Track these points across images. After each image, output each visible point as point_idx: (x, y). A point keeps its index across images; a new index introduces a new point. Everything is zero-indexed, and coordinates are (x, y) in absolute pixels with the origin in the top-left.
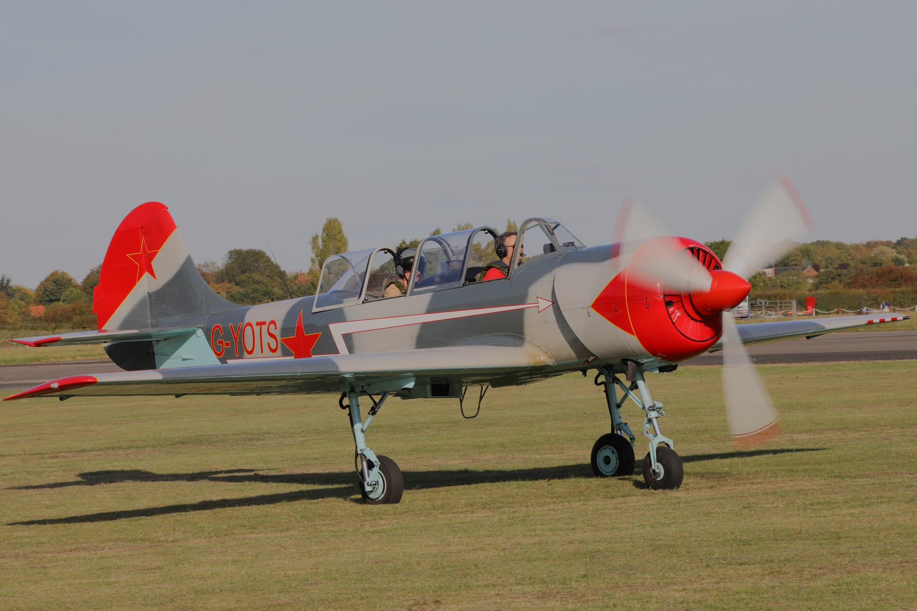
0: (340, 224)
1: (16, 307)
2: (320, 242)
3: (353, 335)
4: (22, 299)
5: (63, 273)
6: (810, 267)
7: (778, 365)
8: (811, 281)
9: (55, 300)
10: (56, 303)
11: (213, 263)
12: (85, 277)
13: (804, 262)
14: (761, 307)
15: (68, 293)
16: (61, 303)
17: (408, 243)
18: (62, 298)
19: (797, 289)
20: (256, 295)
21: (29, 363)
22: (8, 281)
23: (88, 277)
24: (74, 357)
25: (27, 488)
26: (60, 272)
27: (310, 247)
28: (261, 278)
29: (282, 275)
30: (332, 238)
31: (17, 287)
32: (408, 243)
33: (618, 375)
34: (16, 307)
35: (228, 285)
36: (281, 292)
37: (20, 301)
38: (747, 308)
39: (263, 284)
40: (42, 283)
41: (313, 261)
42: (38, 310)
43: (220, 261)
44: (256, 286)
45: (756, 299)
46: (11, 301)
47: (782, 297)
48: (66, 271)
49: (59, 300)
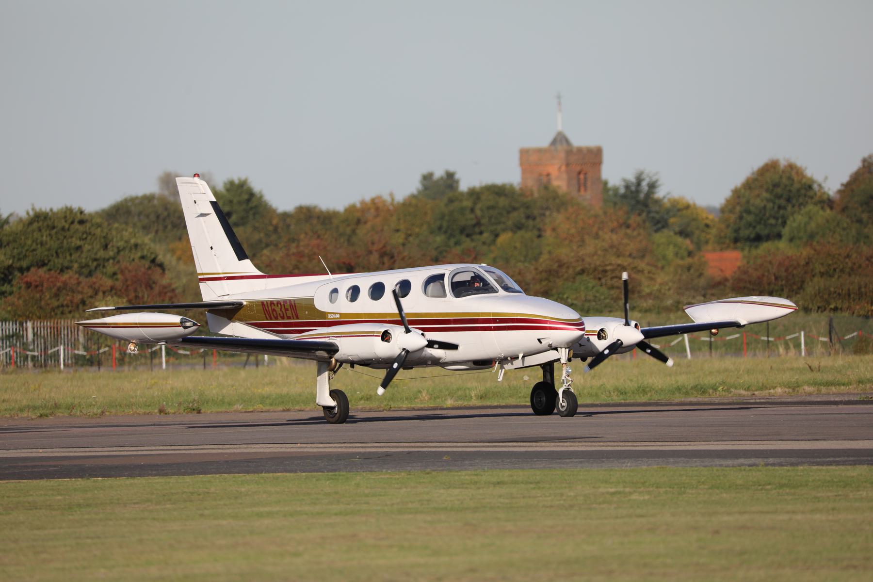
3: (333, 388)
4: (683, 233)
5: (791, 166)
9: (768, 238)
10: (765, 246)
12: (845, 179)
16: (782, 244)
21: (678, 398)
22: (652, 186)
24: (795, 387)
25: (154, 425)
26: (783, 163)
33: (332, 403)
37: (679, 240)
40: (736, 193)
42: (729, 261)
48: (799, 163)
49: (779, 236)
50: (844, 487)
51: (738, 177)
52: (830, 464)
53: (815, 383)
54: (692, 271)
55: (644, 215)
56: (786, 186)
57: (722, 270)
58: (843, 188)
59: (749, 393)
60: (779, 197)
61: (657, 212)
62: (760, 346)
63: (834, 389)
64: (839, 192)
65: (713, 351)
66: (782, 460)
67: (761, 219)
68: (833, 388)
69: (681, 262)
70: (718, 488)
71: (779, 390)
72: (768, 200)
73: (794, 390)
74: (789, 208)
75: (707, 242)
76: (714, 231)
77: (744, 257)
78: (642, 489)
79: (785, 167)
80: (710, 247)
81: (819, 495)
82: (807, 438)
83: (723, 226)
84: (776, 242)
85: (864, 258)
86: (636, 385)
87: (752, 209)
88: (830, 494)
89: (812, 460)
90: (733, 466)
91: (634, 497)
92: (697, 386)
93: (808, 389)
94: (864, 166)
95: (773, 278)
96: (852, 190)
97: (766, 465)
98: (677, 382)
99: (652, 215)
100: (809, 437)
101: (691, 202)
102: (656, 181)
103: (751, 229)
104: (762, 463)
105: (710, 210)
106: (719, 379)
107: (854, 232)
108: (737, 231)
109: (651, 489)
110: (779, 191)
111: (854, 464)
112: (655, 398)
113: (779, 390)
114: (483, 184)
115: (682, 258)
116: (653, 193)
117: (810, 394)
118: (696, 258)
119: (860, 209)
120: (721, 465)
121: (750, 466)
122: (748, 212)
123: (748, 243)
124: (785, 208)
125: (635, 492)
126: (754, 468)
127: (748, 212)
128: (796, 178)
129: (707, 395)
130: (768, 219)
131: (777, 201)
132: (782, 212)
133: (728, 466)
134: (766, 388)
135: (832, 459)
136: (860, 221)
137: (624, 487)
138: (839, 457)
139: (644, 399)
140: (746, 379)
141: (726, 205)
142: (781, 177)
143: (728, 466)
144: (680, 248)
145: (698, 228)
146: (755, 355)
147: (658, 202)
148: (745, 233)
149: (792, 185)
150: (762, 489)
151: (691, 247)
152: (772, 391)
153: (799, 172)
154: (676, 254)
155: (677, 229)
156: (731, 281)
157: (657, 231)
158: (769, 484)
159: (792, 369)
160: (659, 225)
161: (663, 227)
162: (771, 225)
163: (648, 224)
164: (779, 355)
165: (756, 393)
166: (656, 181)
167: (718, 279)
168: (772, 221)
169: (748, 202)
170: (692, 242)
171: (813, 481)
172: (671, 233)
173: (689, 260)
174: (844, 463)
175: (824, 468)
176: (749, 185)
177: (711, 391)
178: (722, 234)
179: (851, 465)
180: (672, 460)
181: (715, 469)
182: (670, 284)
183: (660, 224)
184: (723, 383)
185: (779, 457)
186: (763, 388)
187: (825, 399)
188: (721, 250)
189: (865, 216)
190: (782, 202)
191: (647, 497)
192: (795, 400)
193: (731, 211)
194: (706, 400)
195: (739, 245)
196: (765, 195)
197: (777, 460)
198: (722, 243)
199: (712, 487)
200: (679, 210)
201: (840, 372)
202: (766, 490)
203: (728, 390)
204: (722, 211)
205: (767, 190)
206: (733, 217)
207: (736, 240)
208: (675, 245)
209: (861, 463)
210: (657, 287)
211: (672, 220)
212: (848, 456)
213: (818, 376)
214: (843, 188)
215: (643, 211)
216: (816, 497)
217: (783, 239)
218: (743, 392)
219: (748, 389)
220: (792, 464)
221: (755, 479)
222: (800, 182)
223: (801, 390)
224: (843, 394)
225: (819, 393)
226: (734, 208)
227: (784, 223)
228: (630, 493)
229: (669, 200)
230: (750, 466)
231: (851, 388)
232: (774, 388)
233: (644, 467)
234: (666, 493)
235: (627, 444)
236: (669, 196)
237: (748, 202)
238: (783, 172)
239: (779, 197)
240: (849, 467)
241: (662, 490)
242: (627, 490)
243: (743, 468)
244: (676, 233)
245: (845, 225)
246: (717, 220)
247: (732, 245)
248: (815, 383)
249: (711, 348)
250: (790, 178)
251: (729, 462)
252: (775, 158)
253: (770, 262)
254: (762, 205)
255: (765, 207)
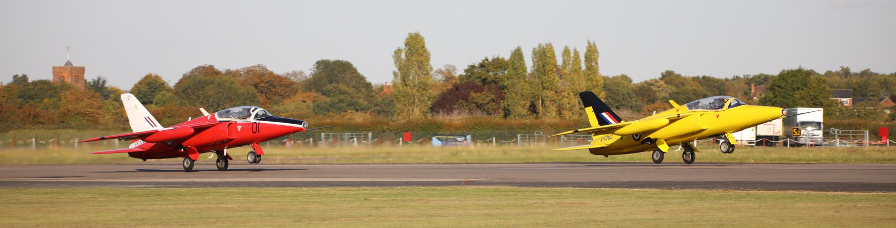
0: (422, 39)
1: (110, 107)
2: (403, 56)
5: (157, 76)
6: (887, 98)
7: (840, 193)
8: (888, 112)
11: (301, 73)
13: (882, 93)
14: (834, 135)
15: (160, 96)
17: (490, 60)
18: (154, 101)
19: (874, 119)
20: (341, 105)
22: (104, 82)
23: (181, 81)
27: (392, 61)
28: (347, 89)
29: (368, 86)
30: (415, 51)
31: (112, 88)
32: (490, 60)
34: (110, 107)
35: (315, 94)
36: (366, 102)
38: (821, 136)
39: (349, 94)
40: (136, 85)
41: (395, 74)
43: (307, 69)
44: (342, 97)
45: (829, 127)
46: (106, 102)
47: (857, 127)
49: (152, 102)
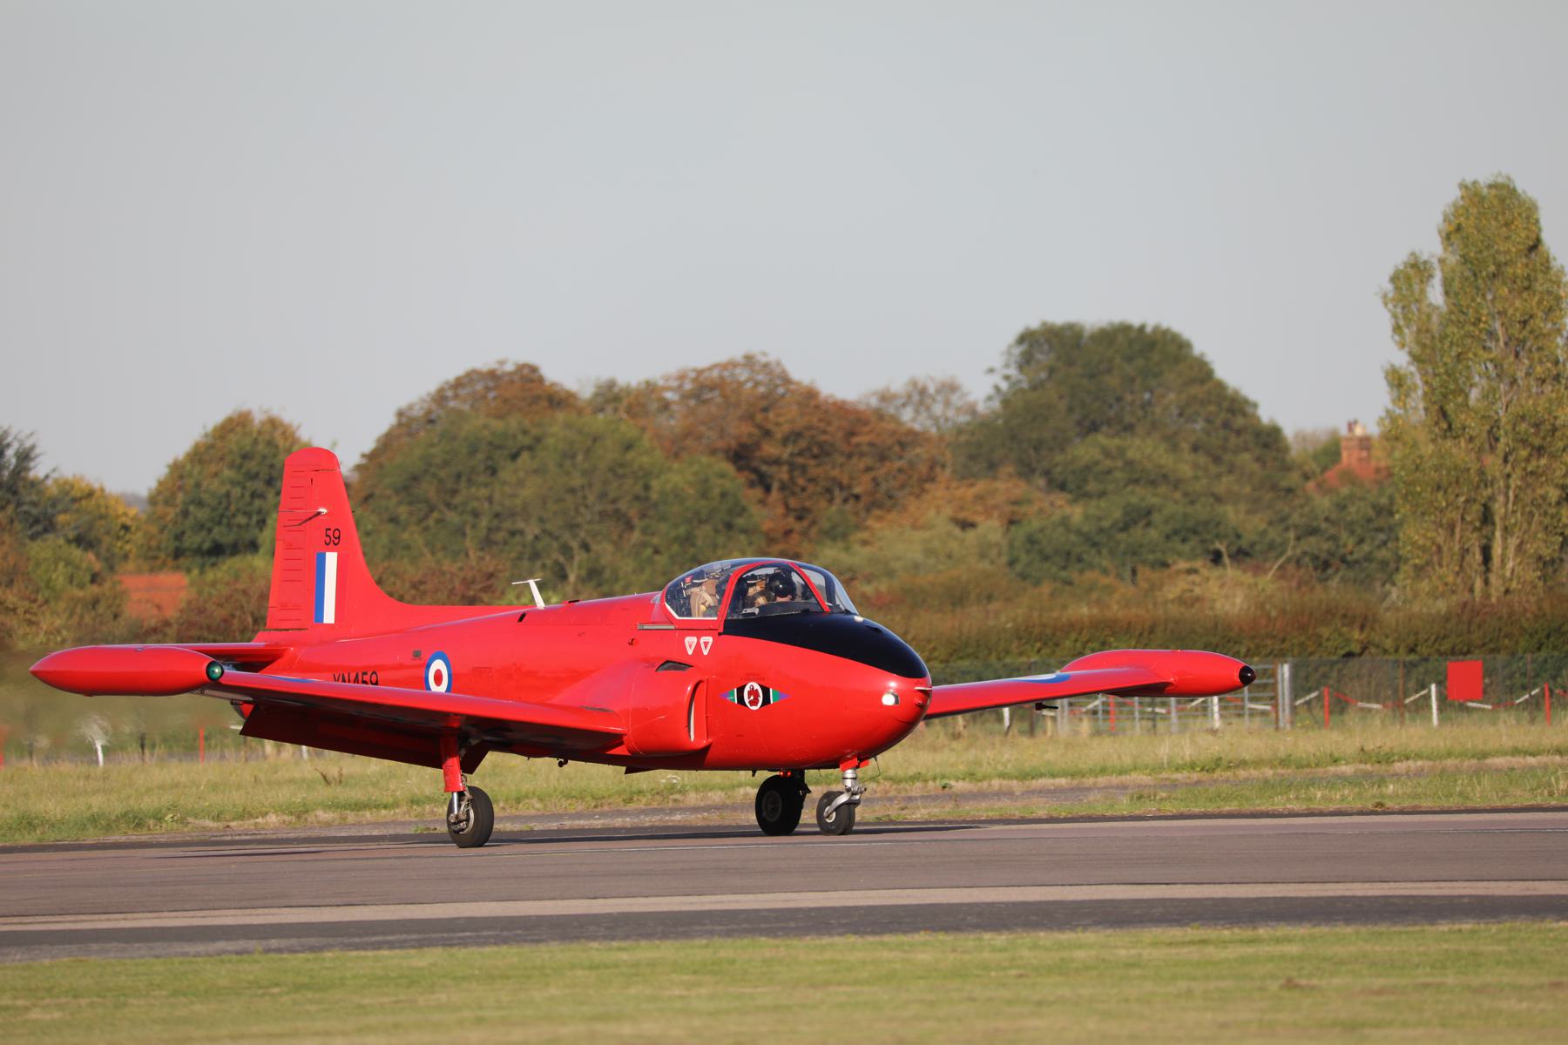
4: (83, 541)
9: (235, 549)
10: (229, 565)
12: (369, 446)
24: (301, 812)
26: (258, 417)
37: (76, 553)
40: (177, 470)
49: (253, 546)
50: (409, 986)
51: (180, 442)
52: (378, 946)
53: (335, 806)
54: (101, 609)
55: (10, 509)
56: (264, 457)
57: (159, 607)
58: (364, 461)
59: (221, 825)
60: (254, 477)
61: (34, 504)
62: (228, 741)
63: (368, 815)
64: (358, 468)
65: (147, 751)
66: (293, 941)
67: (222, 516)
68: (368, 814)
69: (80, 594)
70: (185, 995)
71: (273, 819)
72: (233, 483)
73: (299, 817)
74: (271, 495)
75: (126, 557)
76: (138, 537)
77: (192, 584)
78: (47, 1001)
79: (263, 423)
80: (130, 565)
81: (366, 1001)
82: (333, 901)
83: (154, 529)
84: (249, 557)
85: (407, 585)
86: (15, 815)
87: (205, 497)
88: (385, 1000)
89: (346, 940)
90: (209, 955)
91: (35, 1014)
92: (126, 814)
93: (323, 815)
94: (400, 425)
95: (250, 620)
96: (381, 466)
97: (267, 951)
98: (90, 807)
99: (25, 508)
100: (339, 901)
101: (96, 486)
102: (33, 448)
103: (204, 533)
104: (260, 948)
105: (130, 500)
106: (167, 798)
107: (384, 539)
108: (179, 537)
109: (64, 1000)
110: (252, 466)
111: (421, 944)
112: (51, 837)
113: (273, 819)
114: (210, 428)
115: (81, 586)
116: (27, 469)
117: (328, 825)
118: (107, 585)
119: (394, 500)
120: (186, 954)
121: (238, 953)
122: (200, 504)
123: (198, 560)
124: (262, 496)
125: (35, 1006)
126: (245, 957)
127: (200, 504)
128: (281, 443)
129: (145, 831)
130: (234, 516)
131: (249, 484)
132: (257, 503)
133: (198, 955)
134: (251, 816)
135: (379, 938)
136: (394, 520)
137: (15, 998)
138: (392, 933)
139: (30, 839)
140: (213, 800)
141: (159, 493)
142: (256, 442)
143: (198, 955)
144: (78, 568)
145: (108, 533)
146: (222, 757)
147: (34, 484)
148: (192, 540)
149: (275, 456)
150: (263, 995)
151: (97, 566)
152: (260, 820)
153: (288, 433)
154: (71, 579)
155: (71, 534)
156: (175, 627)
157: (33, 537)
158: (277, 985)
159: (291, 781)
160: (39, 528)
161: (46, 530)
162: (239, 526)
163: (18, 526)
164: (265, 757)
165: (233, 824)
166: (33, 448)
167: (153, 623)
168: (241, 520)
169: (198, 485)
170: (98, 555)
171: (354, 977)
172: (61, 541)
173: (95, 589)
174: (402, 945)
175: (369, 953)
176: (199, 455)
177: (151, 822)
178: (154, 543)
179: (414, 947)
180: (95, 946)
181: (176, 960)
182: (64, 633)
183: (42, 524)
184: (173, 807)
185: (288, 937)
186: (243, 815)
187: (353, 832)
188: (152, 570)
189: (403, 511)
190: (258, 485)
191: (57, 1015)
192: (303, 835)
193: (168, 502)
194: (144, 838)
195: (181, 561)
196: (228, 473)
197: (283, 943)
198: (152, 558)
199: (175, 993)
200: (74, 500)
201: (375, 785)
202: (273, 995)
203: (183, 821)
204: (152, 500)
205: (232, 466)
206: (172, 513)
207: (178, 554)
208: (68, 563)
209: (431, 943)
210: (41, 638)
211: (61, 518)
212: (407, 932)
213: (344, 794)
214: (364, 461)
215: (8, 502)
216: (360, 1006)
217: (262, 551)
218: (209, 823)
219: (217, 818)
220: (312, 949)
221: (251, 977)
222: (288, 450)
223: (311, 818)
224: (385, 824)
225: (343, 822)
226: (173, 495)
227: (262, 523)
228: (27, 1009)
229: (56, 481)
230: (238, 953)
231: (398, 813)
232: (264, 815)
233: (47, 962)
234: (92, 1005)
235: (9, 920)
236: (55, 475)
237: (198, 485)
238: (260, 433)
239: (254, 477)
240: (412, 952)
241: (84, 1002)
242: (20, 1003)
243: (225, 957)
244: (69, 542)
245: (369, 527)
246: (143, 517)
247: (170, 562)
248: (335, 806)
249: (143, 746)
250: (270, 443)
251: (200, 948)
252: (245, 408)
253: (245, 592)
254: (223, 490)
255: (228, 495)
